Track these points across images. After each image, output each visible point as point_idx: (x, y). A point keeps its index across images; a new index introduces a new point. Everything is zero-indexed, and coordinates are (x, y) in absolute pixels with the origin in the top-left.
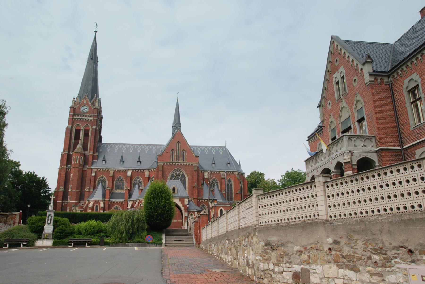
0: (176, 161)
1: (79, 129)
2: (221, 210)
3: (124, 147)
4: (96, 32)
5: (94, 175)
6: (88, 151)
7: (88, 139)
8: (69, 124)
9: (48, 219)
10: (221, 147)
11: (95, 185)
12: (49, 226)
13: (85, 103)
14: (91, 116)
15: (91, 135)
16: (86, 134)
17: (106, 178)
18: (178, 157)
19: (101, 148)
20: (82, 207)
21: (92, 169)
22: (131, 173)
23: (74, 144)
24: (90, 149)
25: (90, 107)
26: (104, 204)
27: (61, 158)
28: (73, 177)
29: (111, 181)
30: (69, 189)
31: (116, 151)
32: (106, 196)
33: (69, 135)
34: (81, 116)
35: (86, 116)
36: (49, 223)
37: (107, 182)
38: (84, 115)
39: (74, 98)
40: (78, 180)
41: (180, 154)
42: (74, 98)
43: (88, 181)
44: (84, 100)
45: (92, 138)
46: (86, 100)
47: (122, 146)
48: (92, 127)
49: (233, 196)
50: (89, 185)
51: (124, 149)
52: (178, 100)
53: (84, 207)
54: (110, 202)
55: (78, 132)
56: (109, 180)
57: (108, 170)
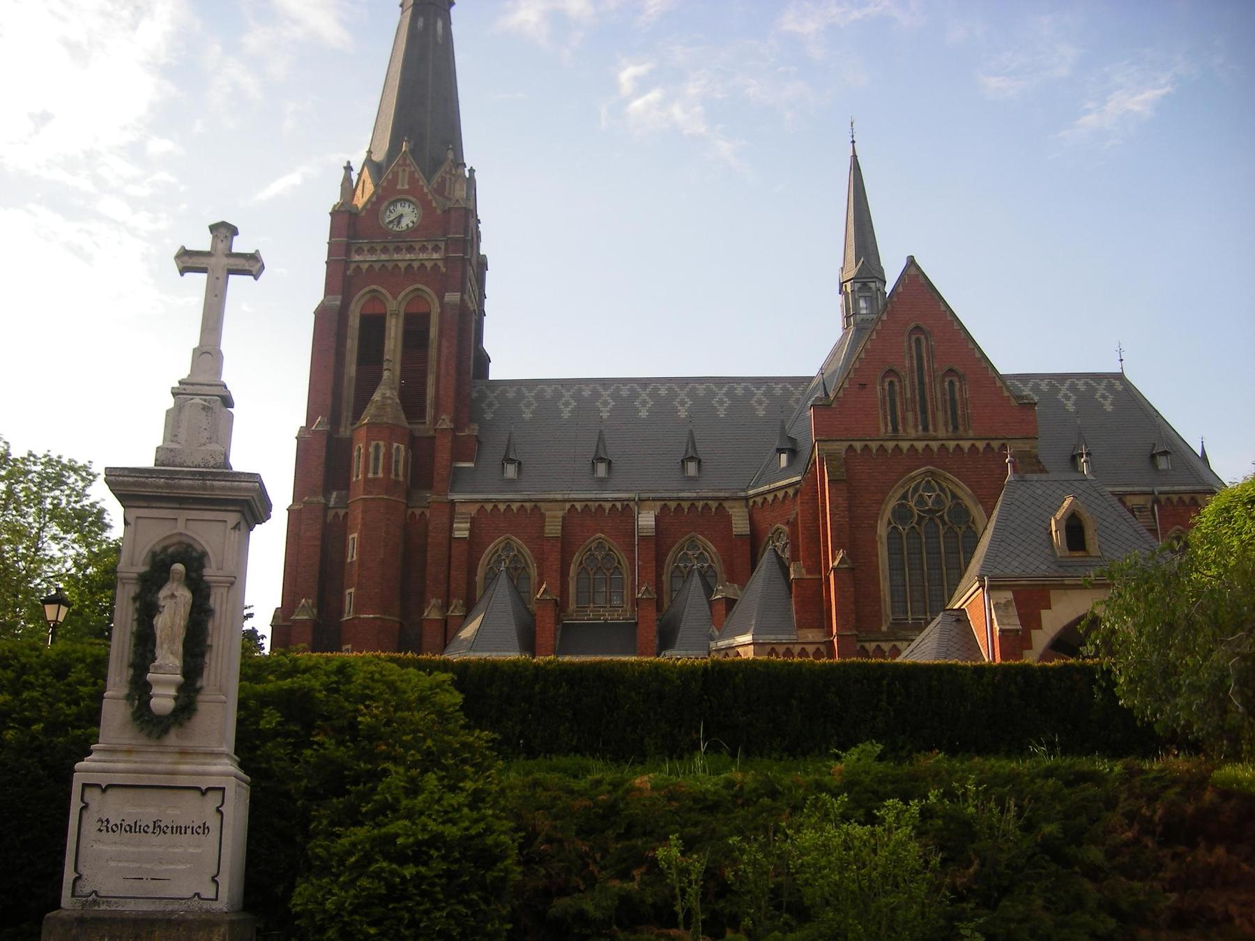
0: (912, 433)
5: (466, 534)
6: (428, 418)
7: (424, 360)
8: (329, 290)
9: (145, 641)
11: (471, 584)
12: (159, 762)
13: (403, 185)
14: (436, 249)
17: (526, 551)
18: (924, 411)
19: (490, 405)
21: (453, 503)
30: (341, 612)
34: (385, 250)
35: (410, 249)
36: (163, 700)
38: (403, 241)
39: (348, 168)
42: (348, 168)
48: (441, 297)
52: (855, 157)
55: (373, 327)
56: (541, 560)
57: (535, 512)
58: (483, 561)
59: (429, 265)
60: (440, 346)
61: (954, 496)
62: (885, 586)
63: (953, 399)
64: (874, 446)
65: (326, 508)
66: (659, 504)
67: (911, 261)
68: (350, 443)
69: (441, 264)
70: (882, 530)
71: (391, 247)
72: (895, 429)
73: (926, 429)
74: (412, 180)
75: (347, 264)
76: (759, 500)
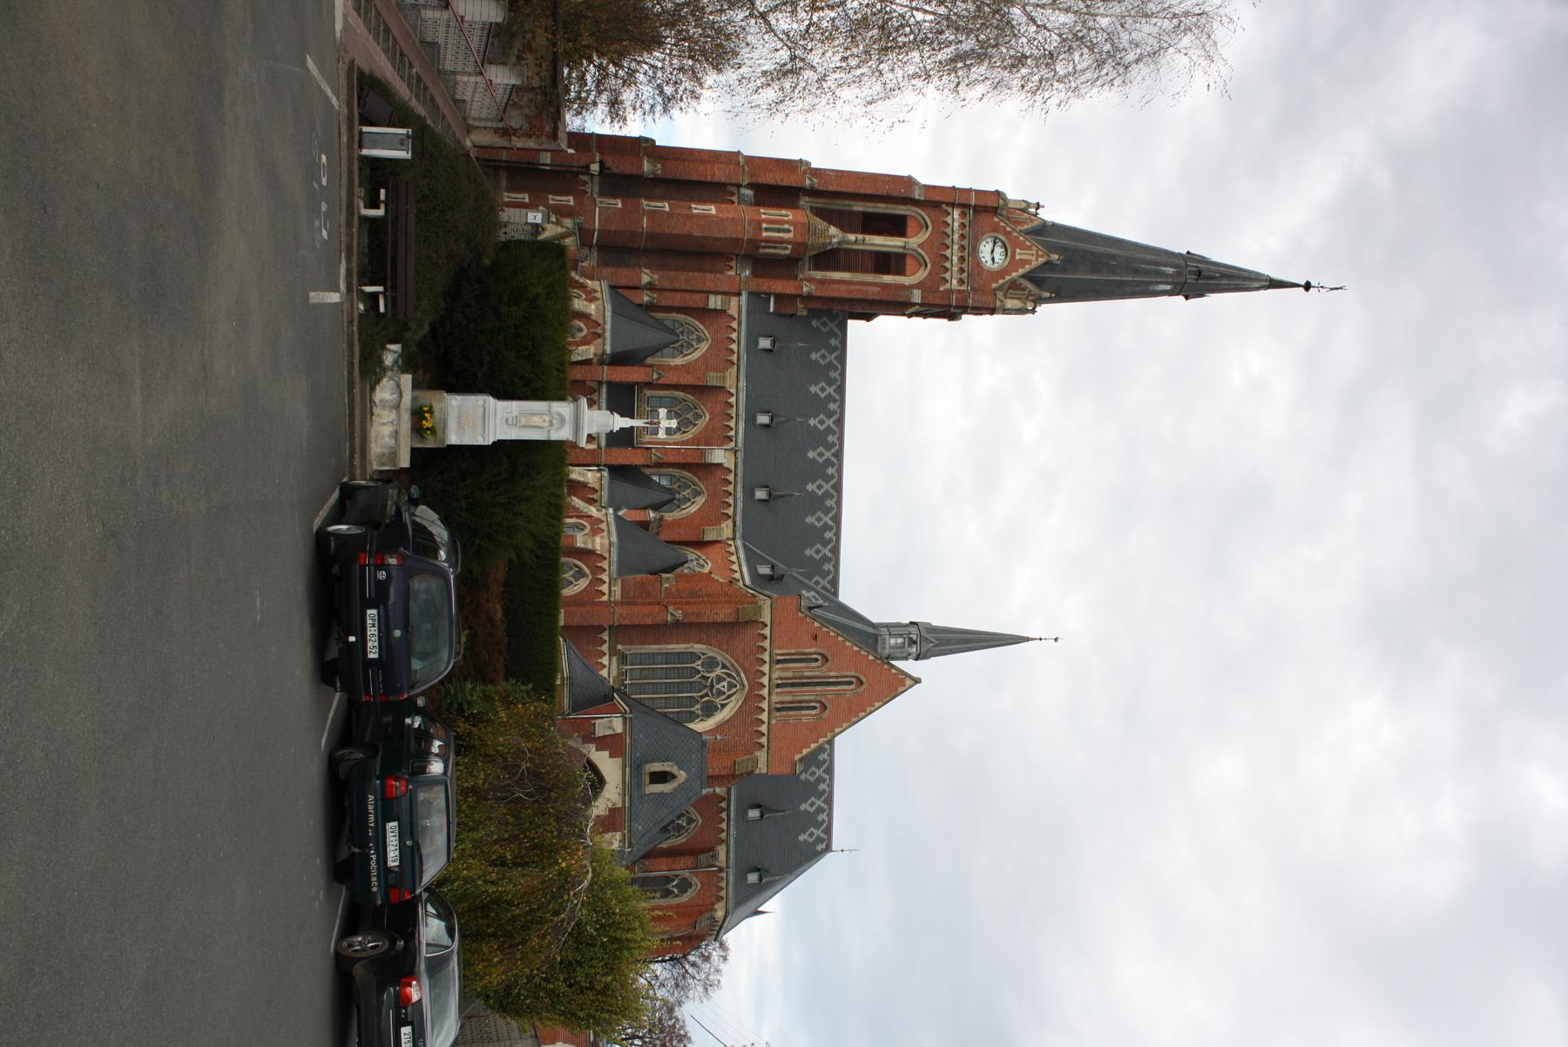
1: (909, 230)
3: (830, 422)
4: (1307, 286)
7: (865, 271)
8: (928, 188)
10: (828, 831)
13: (1020, 255)
15: (885, 286)
16: (886, 262)
17: (696, 355)
18: (793, 685)
21: (739, 294)
23: (841, 213)
24: (822, 282)
26: (587, 362)
27: (784, 161)
32: (619, 369)
33: (883, 190)
34: (962, 237)
35: (962, 259)
37: (679, 361)
40: (690, 236)
41: (808, 694)
43: (684, 278)
44: (1029, 248)
45: (871, 289)
46: (1032, 257)
47: (836, 348)
50: (667, 285)
51: (820, 487)
52: (1028, 639)
54: (595, 385)
55: (896, 226)
56: (687, 368)
59: (948, 276)
60: (876, 284)
61: (723, 706)
62: (653, 648)
63: (802, 708)
64: (766, 644)
65: (739, 186)
66: (732, 467)
67: (917, 681)
68: (793, 206)
69: (947, 286)
70: (698, 648)
71: (965, 243)
72: (779, 662)
73: (778, 686)
74: (1024, 262)
75: (953, 205)
76: (732, 549)
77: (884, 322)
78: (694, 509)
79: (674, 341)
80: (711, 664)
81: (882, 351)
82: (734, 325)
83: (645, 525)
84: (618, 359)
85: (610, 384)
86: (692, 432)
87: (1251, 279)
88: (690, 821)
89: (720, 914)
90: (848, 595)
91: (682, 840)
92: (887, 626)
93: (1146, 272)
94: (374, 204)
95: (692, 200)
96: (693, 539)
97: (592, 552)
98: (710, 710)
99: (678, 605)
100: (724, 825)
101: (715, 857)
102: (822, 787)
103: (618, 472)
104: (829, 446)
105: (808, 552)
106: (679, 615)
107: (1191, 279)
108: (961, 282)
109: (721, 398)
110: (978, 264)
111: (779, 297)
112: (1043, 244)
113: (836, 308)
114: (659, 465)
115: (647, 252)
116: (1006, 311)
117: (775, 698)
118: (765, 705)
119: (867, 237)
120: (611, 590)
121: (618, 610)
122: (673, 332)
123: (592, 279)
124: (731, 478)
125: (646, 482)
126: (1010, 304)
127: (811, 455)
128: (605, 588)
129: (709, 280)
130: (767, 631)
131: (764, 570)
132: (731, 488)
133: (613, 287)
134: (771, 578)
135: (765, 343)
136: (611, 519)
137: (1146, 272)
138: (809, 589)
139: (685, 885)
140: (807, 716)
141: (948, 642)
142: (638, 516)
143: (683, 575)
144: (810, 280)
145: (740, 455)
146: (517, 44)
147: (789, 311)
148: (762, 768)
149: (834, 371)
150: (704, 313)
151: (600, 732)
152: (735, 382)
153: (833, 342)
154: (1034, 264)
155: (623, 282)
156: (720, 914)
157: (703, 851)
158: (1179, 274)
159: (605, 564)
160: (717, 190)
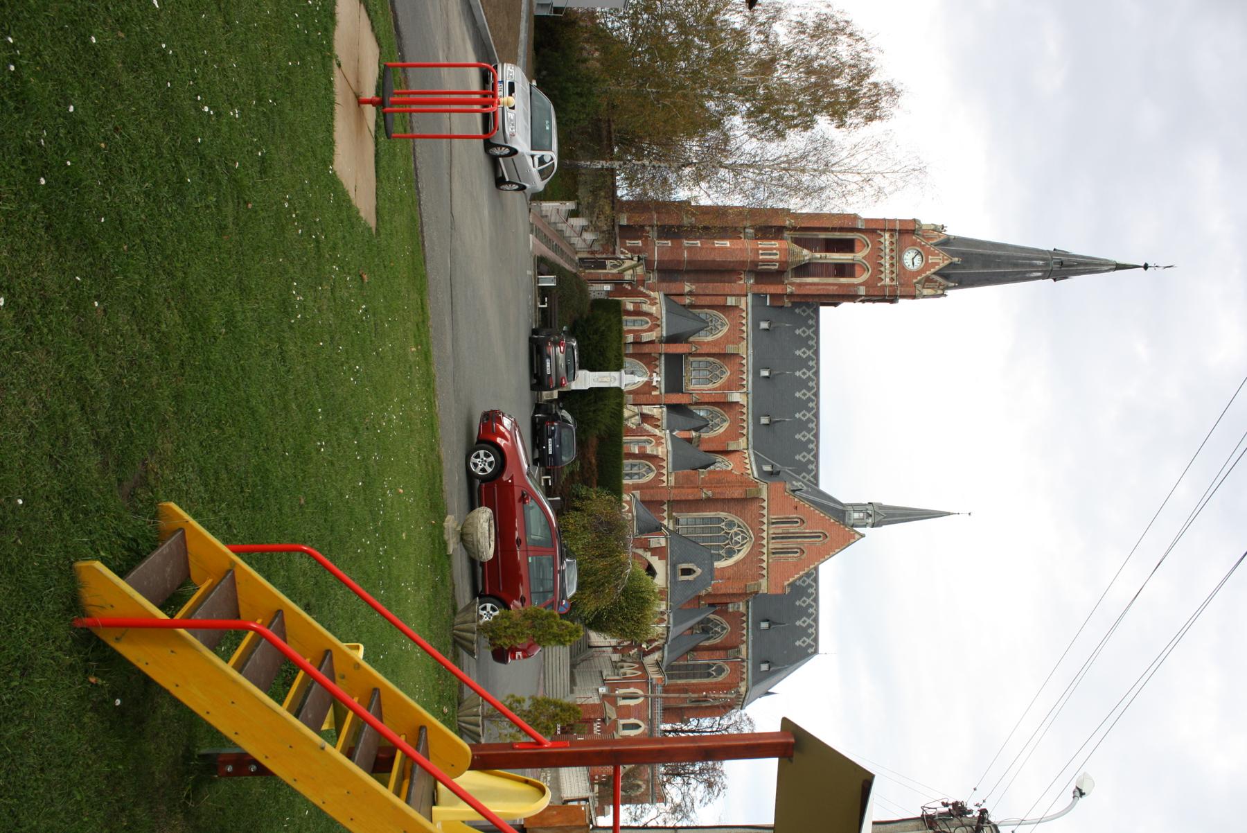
1: (856, 248)
2: (638, 726)
3: (810, 374)
4: (1146, 267)
8: (867, 221)
16: (843, 270)
17: (720, 334)
20: (642, 282)
22: (737, 403)
24: (800, 285)
25: (919, 272)
26: (652, 342)
28: (722, 248)
29: (713, 351)
31: (798, 353)
34: (892, 250)
35: (892, 265)
38: (897, 259)
43: (711, 287)
46: (940, 260)
47: (812, 326)
49: (679, 682)
52: (949, 514)
53: (642, 289)
55: (848, 246)
56: (715, 343)
58: (716, 312)
59: (883, 276)
64: (765, 512)
67: (863, 536)
74: (935, 264)
75: (884, 230)
77: (846, 306)
78: (722, 430)
79: (704, 326)
80: (731, 524)
81: (845, 329)
82: (744, 314)
83: (689, 440)
84: (671, 339)
85: (666, 354)
86: (719, 383)
87: (1101, 265)
88: (723, 628)
89: (743, 689)
90: (826, 485)
91: (717, 641)
92: (851, 505)
93: (1023, 265)
94: (543, 303)
95: (715, 238)
96: (721, 449)
97: (656, 457)
98: (730, 553)
99: (709, 488)
100: (745, 632)
101: (739, 652)
102: (811, 610)
103: (673, 408)
104: (810, 389)
105: (797, 457)
106: (702, 490)
107: (1056, 267)
108: (892, 279)
109: (737, 361)
110: (903, 267)
111: (772, 296)
112: (947, 251)
113: (810, 300)
114: (696, 404)
115: (688, 272)
116: (924, 297)
117: (771, 546)
118: (765, 550)
119: (828, 255)
120: (669, 479)
121: (673, 491)
122: (703, 321)
123: (654, 291)
124: (745, 410)
125: (691, 414)
126: (925, 292)
127: (797, 395)
128: (665, 478)
129: (727, 287)
130: (765, 504)
131: (767, 468)
132: (744, 417)
133: (666, 295)
134: (771, 473)
135: (764, 325)
136: (668, 436)
137: (1023, 265)
138: (798, 480)
139: (720, 670)
140: (792, 558)
141: (893, 515)
142: (686, 435)
143: (714, 471)
144: (792, 284)
145: (750, 396)
146: (597, 211)
147: (780, 304)
148: (764, 590)
149: (812, 342)
150: (724, 308)
151: (652, 545)
152: (746, 351)
153: (810, 322)
154: (942, 265)
155: (674, 292)
156: (743, 689)
157: (731, 648)
158: (1047, 265)
159: (664, 464)
160: (730, 232)
